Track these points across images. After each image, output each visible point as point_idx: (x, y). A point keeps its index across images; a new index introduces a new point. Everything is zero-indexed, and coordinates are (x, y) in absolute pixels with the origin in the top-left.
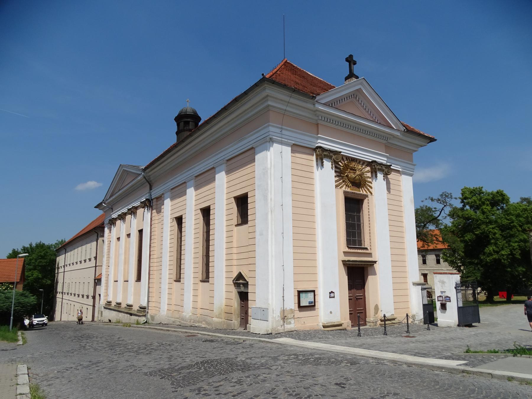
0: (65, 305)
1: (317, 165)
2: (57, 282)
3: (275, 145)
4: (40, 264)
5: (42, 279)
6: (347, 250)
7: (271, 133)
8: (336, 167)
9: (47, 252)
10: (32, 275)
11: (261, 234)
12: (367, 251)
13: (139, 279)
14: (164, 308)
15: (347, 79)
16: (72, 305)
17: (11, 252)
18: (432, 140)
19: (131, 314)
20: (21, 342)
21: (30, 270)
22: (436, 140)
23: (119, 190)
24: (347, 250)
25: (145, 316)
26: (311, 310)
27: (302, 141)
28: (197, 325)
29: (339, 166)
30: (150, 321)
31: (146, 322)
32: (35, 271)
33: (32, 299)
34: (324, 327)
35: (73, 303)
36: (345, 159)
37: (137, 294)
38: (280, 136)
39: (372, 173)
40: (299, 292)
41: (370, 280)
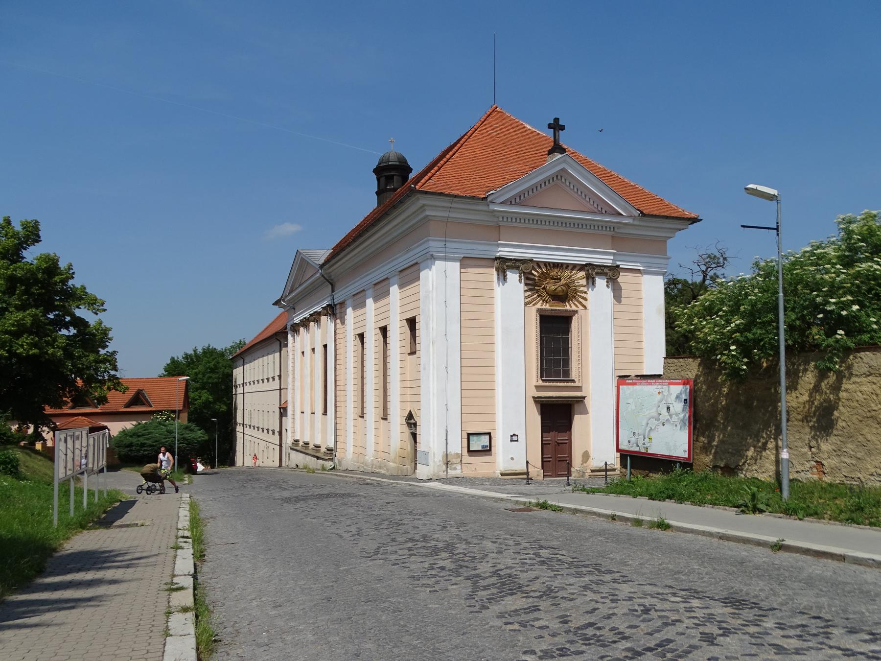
0: (247, 443)
1: (498, 279)
2: (236, 409)
3: (437, 262)
4: (210, 381)
5: (214, 402)
6: (540, 383)
7: (431, 249)
8: (527, 278)
9: (218, 363)
10: (200, 397)
11: (424, 369)
12: (573, 384)
13: (325, 413)
14: (351, 450)
15: (550, 152)
16: (256, 444)
17: (169, 362)
18: (695, 220)
19: (318, 458)
20: (186, 482)
21: (197, 389)
22: (701, 220)
23: (300, 285)
24: (540, 383)
25: (332, 460)
26: (485, 455)
27: (473, 252)
28: (377, 471)
29: (532, 277)
30: (338, 467)
31: (334, 468)
32: (203, 392)
33: (199, 434)
34: (502, 475)
35: (257, 441)
36: (542, 266)
37: (324, 432)
38: (443, 250)
39: (587, 279)
40: (469, 435)
41: (578, 420)
